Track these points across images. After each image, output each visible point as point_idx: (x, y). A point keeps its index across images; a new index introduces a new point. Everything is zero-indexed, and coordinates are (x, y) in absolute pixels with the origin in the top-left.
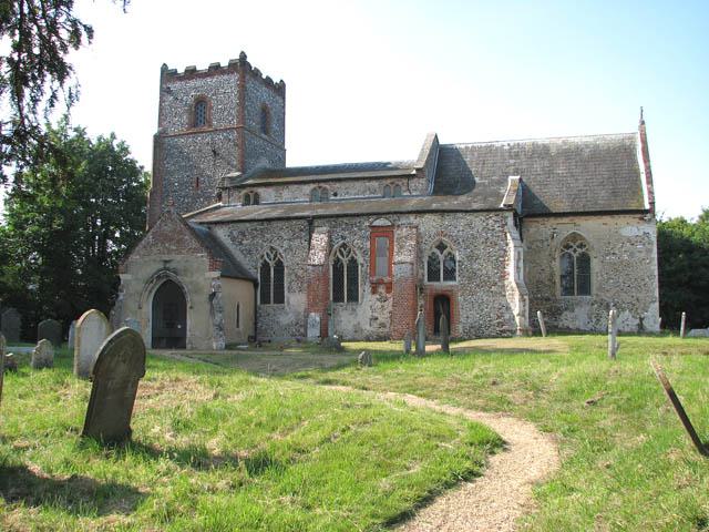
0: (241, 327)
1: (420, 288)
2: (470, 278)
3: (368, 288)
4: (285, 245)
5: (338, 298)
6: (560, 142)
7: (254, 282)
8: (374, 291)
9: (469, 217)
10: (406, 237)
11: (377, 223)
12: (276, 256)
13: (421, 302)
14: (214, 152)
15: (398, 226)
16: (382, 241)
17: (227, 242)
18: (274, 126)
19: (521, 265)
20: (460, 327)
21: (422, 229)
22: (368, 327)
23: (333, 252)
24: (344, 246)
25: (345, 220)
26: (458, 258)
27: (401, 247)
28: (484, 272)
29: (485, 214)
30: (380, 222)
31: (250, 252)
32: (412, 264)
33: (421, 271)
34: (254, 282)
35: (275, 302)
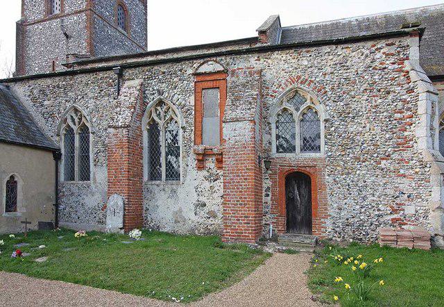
0: (21, 211)
1: (264, 162)
2: (344, 147)
3: (192, 161)
4: (91, 103)
5: (154, 175)
6: (418, 11)
7: (57, 155)
8: (201, 165)
9: (340, 50)
10: (244, 86)
11: (206, 68)
12: (80, 119)
13: (267, 183)
14: (65, 34)
15: (233, 71)
16: (212, 96)
17: (27, 103)
18: (135, 26)
19: (436, 124)
20: (329, 222)
21: (268, 76)
22: (193, 216)
23: (146, 114)
24: (161, 103)
25: (163, 68)
26: (323, 116)
27: (237, 99)
28: (367, 137)
29: (370, 44)
30: (208, 67)
31: (52, 115)
32: (253, 121)
33: (266, 138)
34: (57, 155)
35: (79, 180)
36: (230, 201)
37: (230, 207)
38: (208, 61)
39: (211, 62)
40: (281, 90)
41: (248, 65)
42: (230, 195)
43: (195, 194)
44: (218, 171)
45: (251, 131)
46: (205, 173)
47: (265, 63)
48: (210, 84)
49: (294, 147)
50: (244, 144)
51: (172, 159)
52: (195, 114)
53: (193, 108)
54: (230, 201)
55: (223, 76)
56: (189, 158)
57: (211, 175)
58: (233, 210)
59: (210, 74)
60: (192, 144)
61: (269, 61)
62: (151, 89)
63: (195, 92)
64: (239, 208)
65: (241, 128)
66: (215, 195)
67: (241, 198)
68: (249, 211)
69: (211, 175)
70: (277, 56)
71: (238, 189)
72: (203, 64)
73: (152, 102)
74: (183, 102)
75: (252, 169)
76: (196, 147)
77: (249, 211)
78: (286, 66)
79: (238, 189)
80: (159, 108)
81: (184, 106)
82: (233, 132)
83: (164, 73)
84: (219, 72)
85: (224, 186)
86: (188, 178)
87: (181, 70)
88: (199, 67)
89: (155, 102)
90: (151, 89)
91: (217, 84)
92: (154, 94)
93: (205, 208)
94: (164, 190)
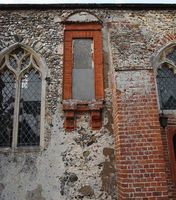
3: (58, 120)
8: (70, 125)
36: (132, 172)
37: (132, 181)
38: (80, 12)
39: (84, 13)
40: (159, 45)
41: (123, 20)
42: (130, 163)
43: (62, 164)
44: (94, 132)
45: (151, 82)
46: (76, 135)
47: (140, 19)
48: (81, 34)
49: (39, 138)
50: (144, 97)
51: (30, 119)
52: (64, 64)
53: (62, 58)
54: (132, 172)
55: (98, 27)
56: (54, 116)
57: (84, 137)
58: (138, 185)
59: (84, 23)
60: (59, 99)
61: (143, 18)
62: (6, 34)
63: (64, 41)
64: (145, 180)
65: (138, 77)
66: (91, 164)
67: (146, 166)
68: (159, 184)
69: (84, 137)
70: (151, 15)
71: (141, 153)
72: (74, 13)
73: (6, 48)
74: (49, 51)
75: (157, 127)
76: (65, 102)
77: (159, 184)
78: (162, 24)
79: (141, 153)
80: (15, 56)
81: (50, 54)
82: (129, 83)
83: (25, 19)
84: (93, 23)
85: (122, 150)
86: (52, 141)
87: (46, 18)
88: (69, 16)
89: (10, 49)
90: (6, 34)
91: (91, 34)
92: (9, 40)
93: (77, 184)
94: (15, 160)
